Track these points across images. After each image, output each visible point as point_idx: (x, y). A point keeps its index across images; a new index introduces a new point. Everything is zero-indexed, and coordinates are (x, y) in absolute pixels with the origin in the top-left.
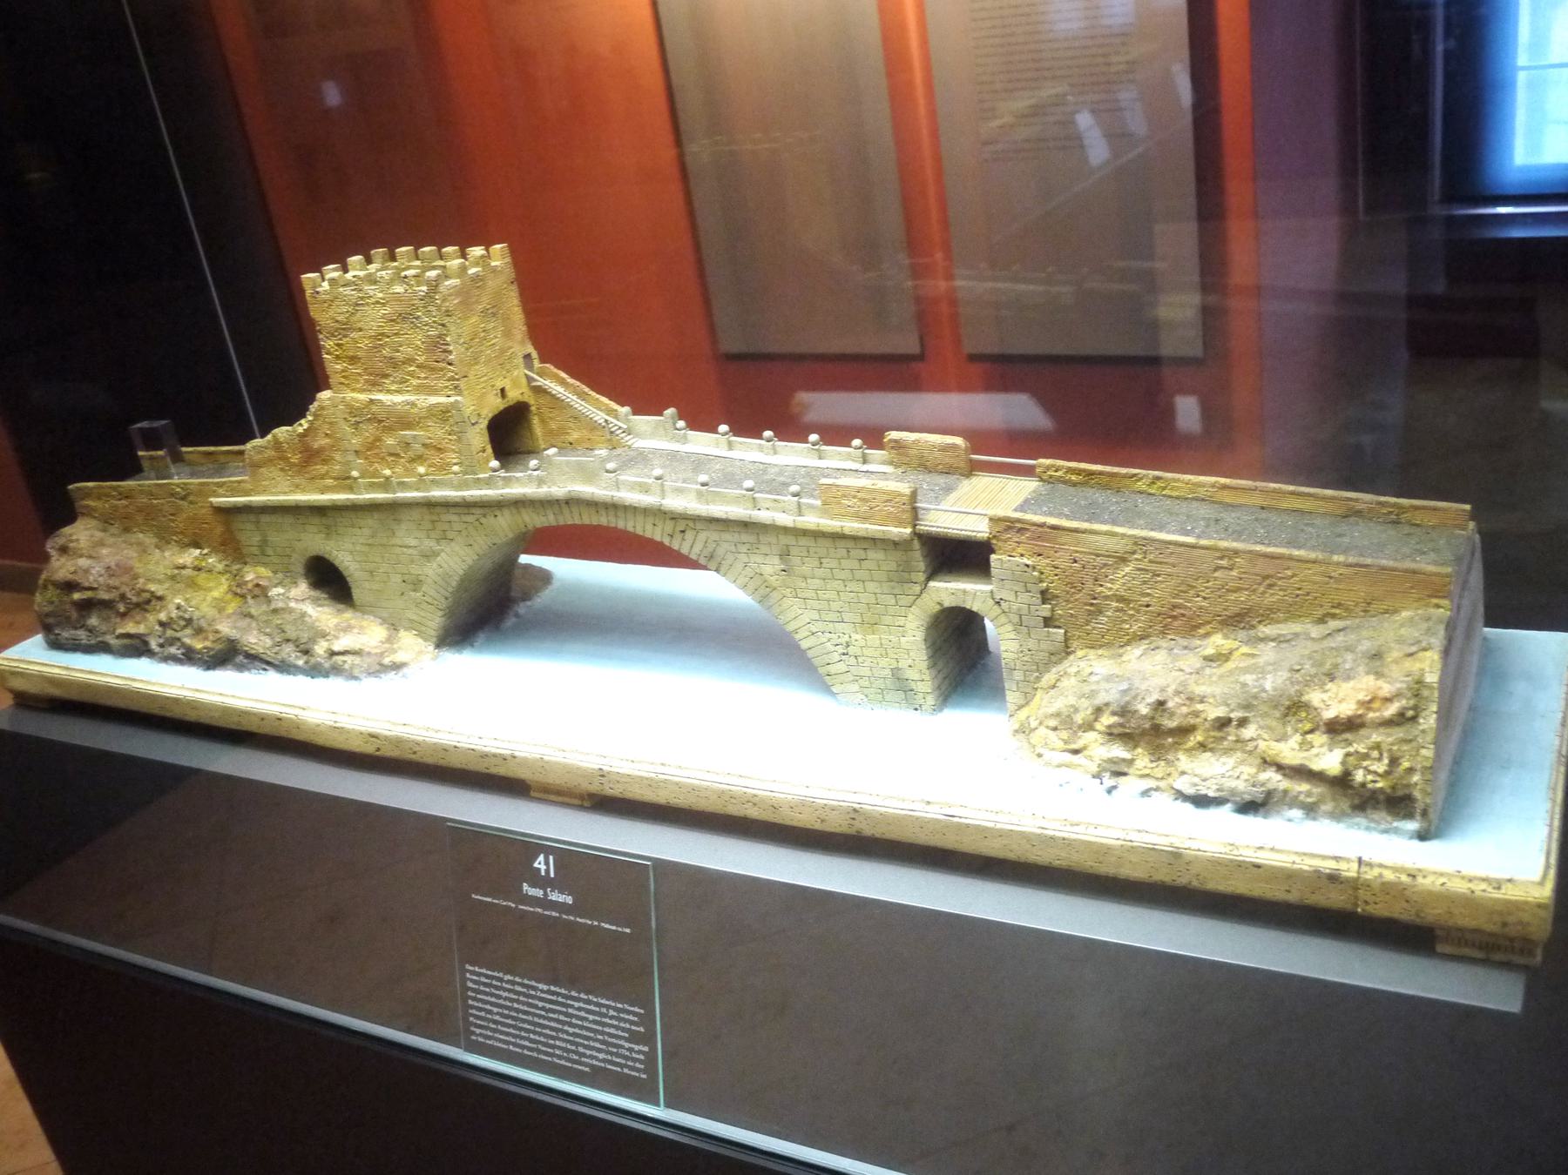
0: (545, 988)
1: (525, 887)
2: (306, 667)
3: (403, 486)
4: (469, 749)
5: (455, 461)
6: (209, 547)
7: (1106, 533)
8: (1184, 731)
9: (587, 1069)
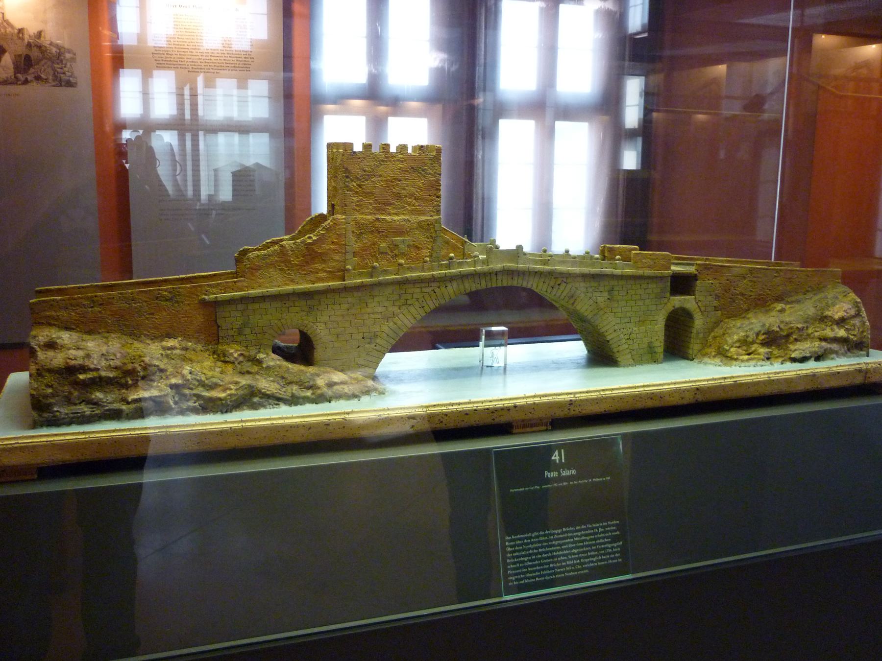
0: (559, 531)
1: (546, 473)
2: (313, 396)
3: (386, 272)
4: (485, 409)
5: (427, 255)
6: (181, 336)
7: (739, 267)
8: (788, 336)
9: (587, 571)
